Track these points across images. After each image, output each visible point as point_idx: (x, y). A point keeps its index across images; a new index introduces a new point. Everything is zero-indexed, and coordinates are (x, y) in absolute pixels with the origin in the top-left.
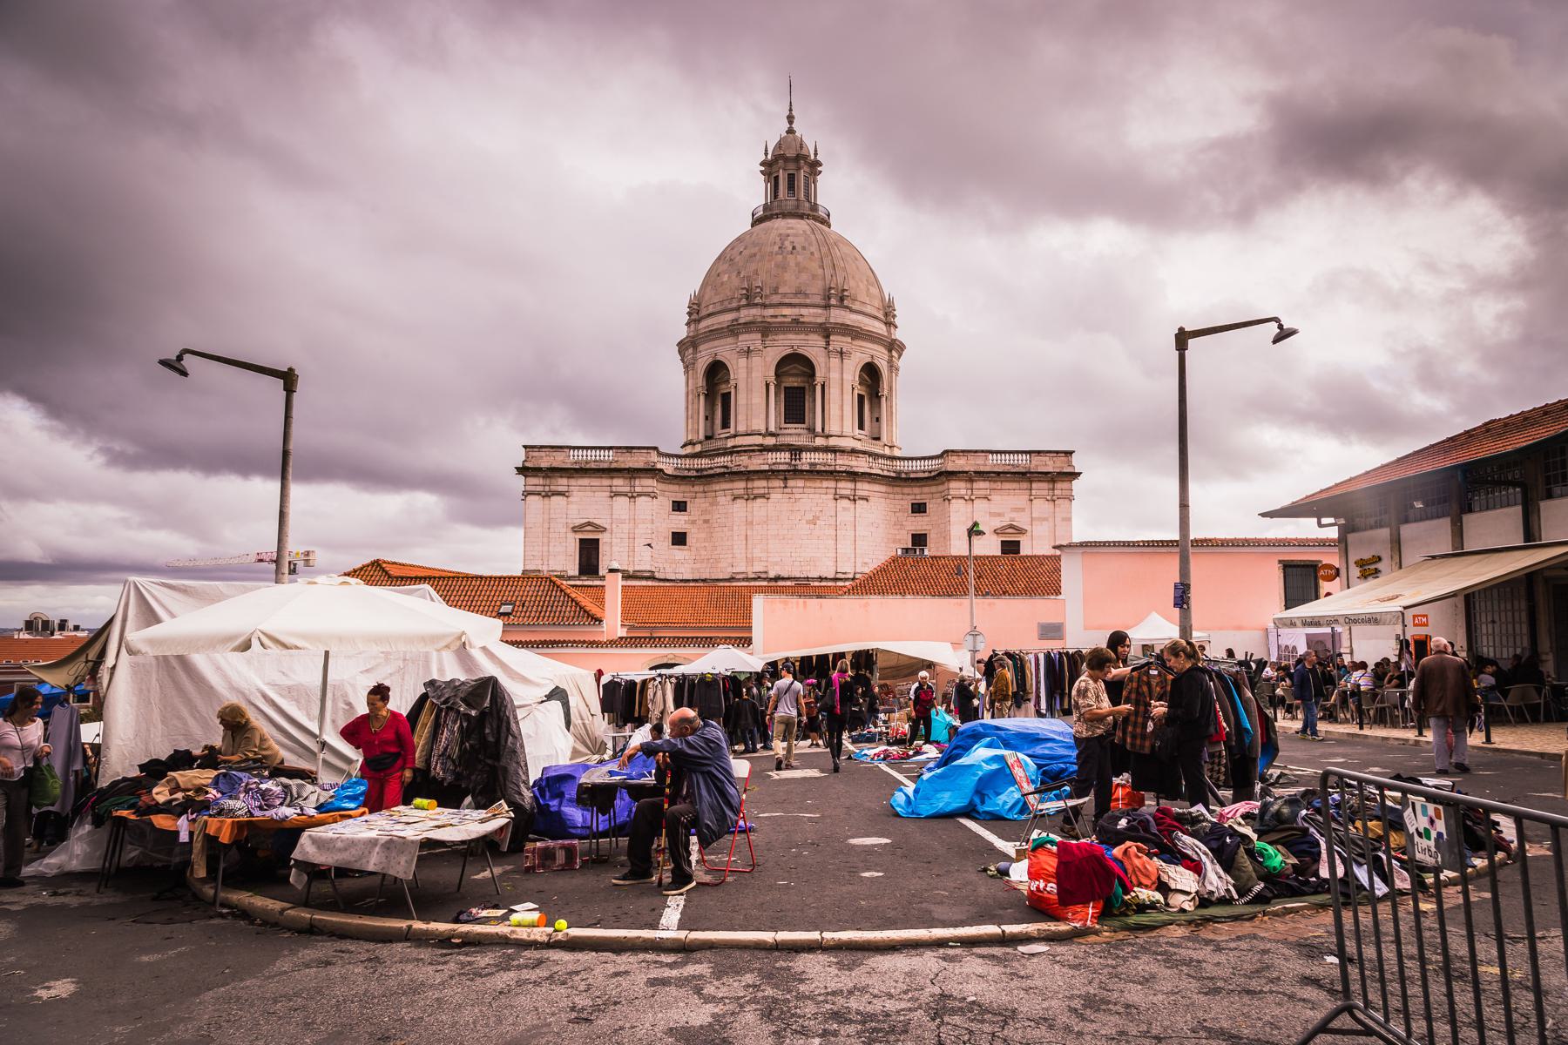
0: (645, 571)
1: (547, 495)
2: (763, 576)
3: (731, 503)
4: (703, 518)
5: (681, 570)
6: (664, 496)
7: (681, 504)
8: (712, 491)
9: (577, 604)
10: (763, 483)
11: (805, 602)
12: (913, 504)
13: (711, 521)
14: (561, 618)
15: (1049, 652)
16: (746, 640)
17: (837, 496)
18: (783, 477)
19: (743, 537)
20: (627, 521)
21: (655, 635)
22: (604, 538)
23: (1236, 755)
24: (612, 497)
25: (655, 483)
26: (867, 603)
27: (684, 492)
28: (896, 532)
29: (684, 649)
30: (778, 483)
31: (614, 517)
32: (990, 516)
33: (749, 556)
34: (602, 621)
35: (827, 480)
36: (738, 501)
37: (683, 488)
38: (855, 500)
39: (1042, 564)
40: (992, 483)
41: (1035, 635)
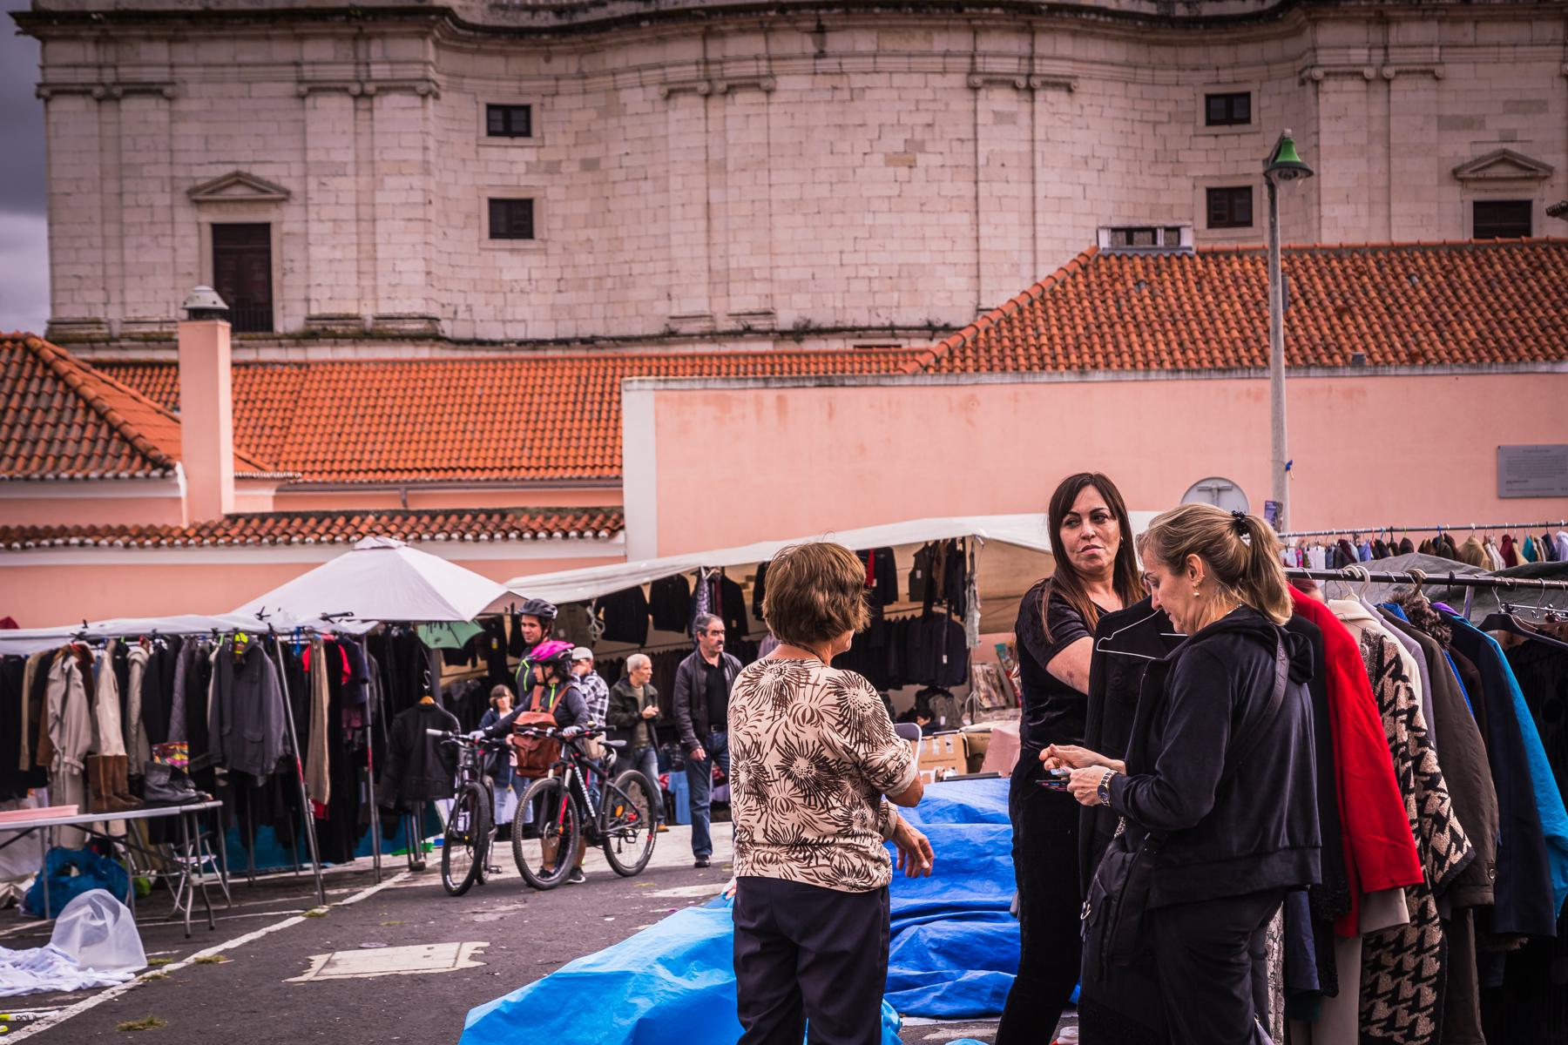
0: (410, 318)
1: (110, 95)
2: (761, 324)
3: (660, 107)
4: (578, 154)
5: (523, 312)
6: (460, 90)
7: (515, 116)
8: (604, 73)
9: (101, 417)
11: (781, 401)
12: (1209, 98)
13: (603, 165)
14: (50, 461)
15: (1343, 544)
16: (607, 517)
17: (978, 80)
18: (812, 25)
19: (699, 210)
20: (350, 169)
21: (413, 507)
22: (285, 221)
23: (1511, 937)
24: (302, 97)
25: (431, 53)
26: (973, 397)
28: (1160, 184)
29: (461, 546)
32: (1440, 128)
33: (718, 264)
34: (170, 467)
35: (947, 28)
36: (682, 100)
37: (518, 65)
38: (1031, 90)
39: (1542, 266)
40: (1446, 27)
41: (1488, 483)
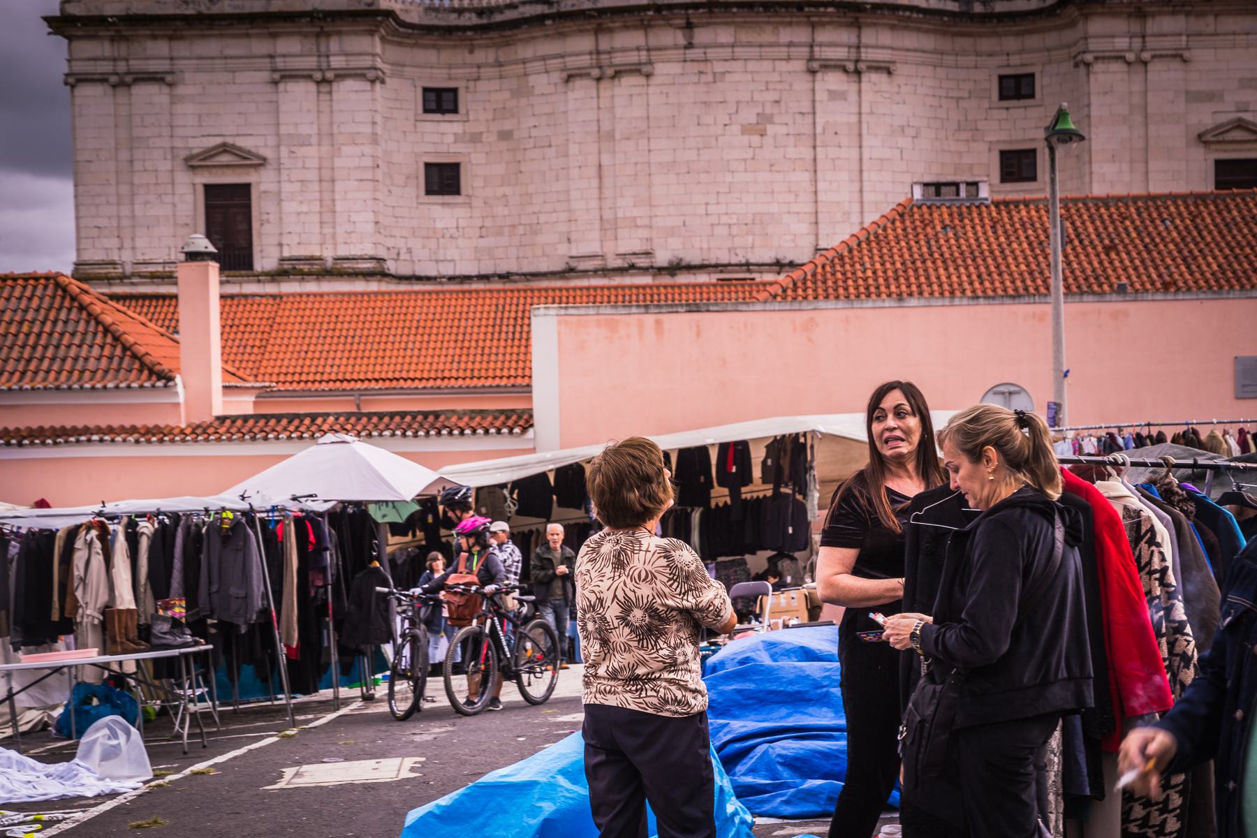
1: (123, 82)
2: (642, 262)
3: (561, 88)
5: (452, 253)
6: (401, 76)
7: (445, 96)
8: (516, 62)
9: (116, 339)
10: (636, 38)
11: (658, 323)
12: (1002, 78)
13: (516, 135)
15: (1111, 436)
16: (520, 417)
17: (815, 65)
19: (592, 171)
20: (314, 140)
22: (261, 182)
24: (275, 83)
25: (379, 49)
26: (812, 320)
27: (450, 67)
28: (962, 147)
29: (403, 441)
30: (670, 37)
31: (283, 130)
32: (1188, 101)
33: (608, 215)
34: (171, 379)
36: (578, 83)
37: (448, 56)
40: (1192, 19)
